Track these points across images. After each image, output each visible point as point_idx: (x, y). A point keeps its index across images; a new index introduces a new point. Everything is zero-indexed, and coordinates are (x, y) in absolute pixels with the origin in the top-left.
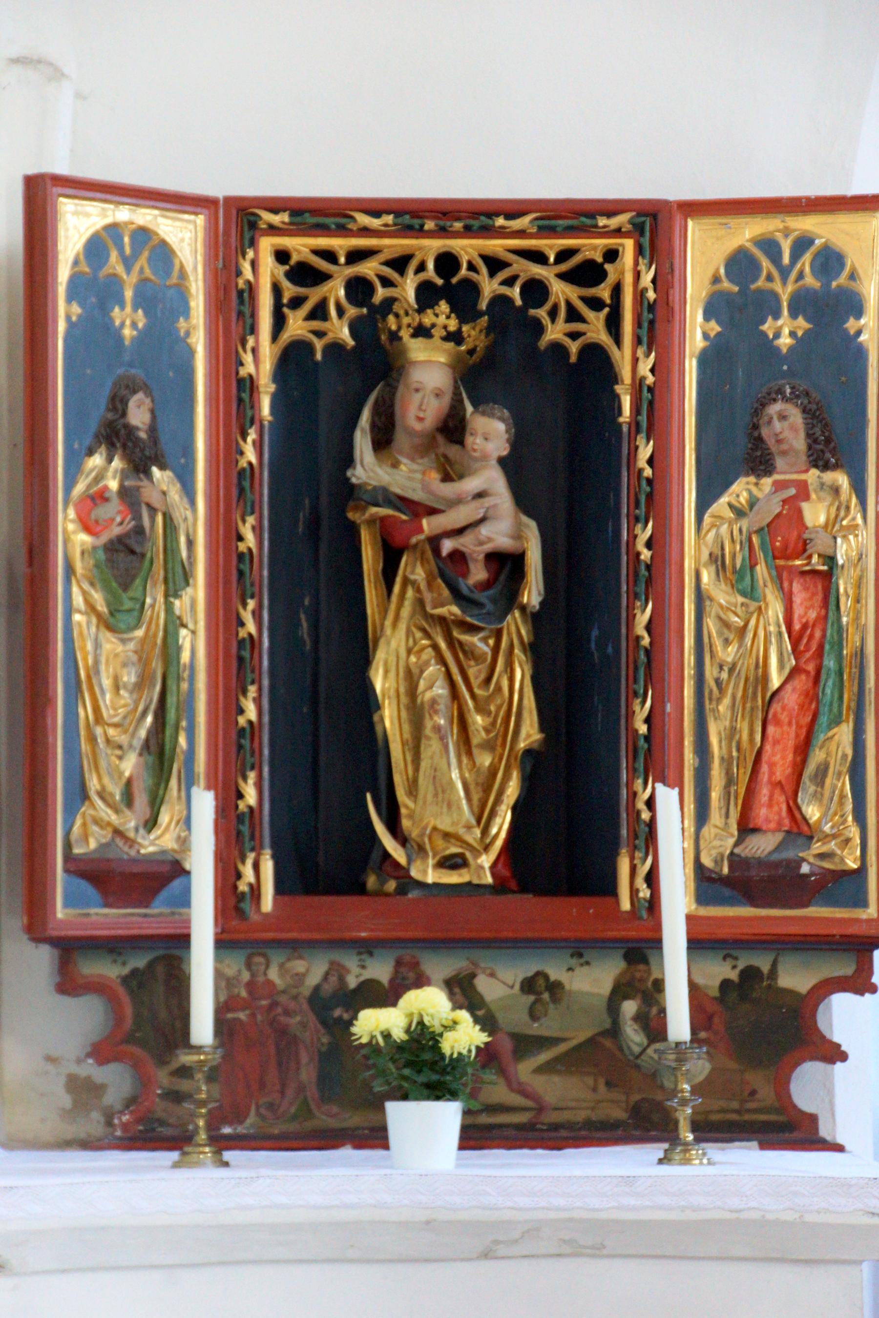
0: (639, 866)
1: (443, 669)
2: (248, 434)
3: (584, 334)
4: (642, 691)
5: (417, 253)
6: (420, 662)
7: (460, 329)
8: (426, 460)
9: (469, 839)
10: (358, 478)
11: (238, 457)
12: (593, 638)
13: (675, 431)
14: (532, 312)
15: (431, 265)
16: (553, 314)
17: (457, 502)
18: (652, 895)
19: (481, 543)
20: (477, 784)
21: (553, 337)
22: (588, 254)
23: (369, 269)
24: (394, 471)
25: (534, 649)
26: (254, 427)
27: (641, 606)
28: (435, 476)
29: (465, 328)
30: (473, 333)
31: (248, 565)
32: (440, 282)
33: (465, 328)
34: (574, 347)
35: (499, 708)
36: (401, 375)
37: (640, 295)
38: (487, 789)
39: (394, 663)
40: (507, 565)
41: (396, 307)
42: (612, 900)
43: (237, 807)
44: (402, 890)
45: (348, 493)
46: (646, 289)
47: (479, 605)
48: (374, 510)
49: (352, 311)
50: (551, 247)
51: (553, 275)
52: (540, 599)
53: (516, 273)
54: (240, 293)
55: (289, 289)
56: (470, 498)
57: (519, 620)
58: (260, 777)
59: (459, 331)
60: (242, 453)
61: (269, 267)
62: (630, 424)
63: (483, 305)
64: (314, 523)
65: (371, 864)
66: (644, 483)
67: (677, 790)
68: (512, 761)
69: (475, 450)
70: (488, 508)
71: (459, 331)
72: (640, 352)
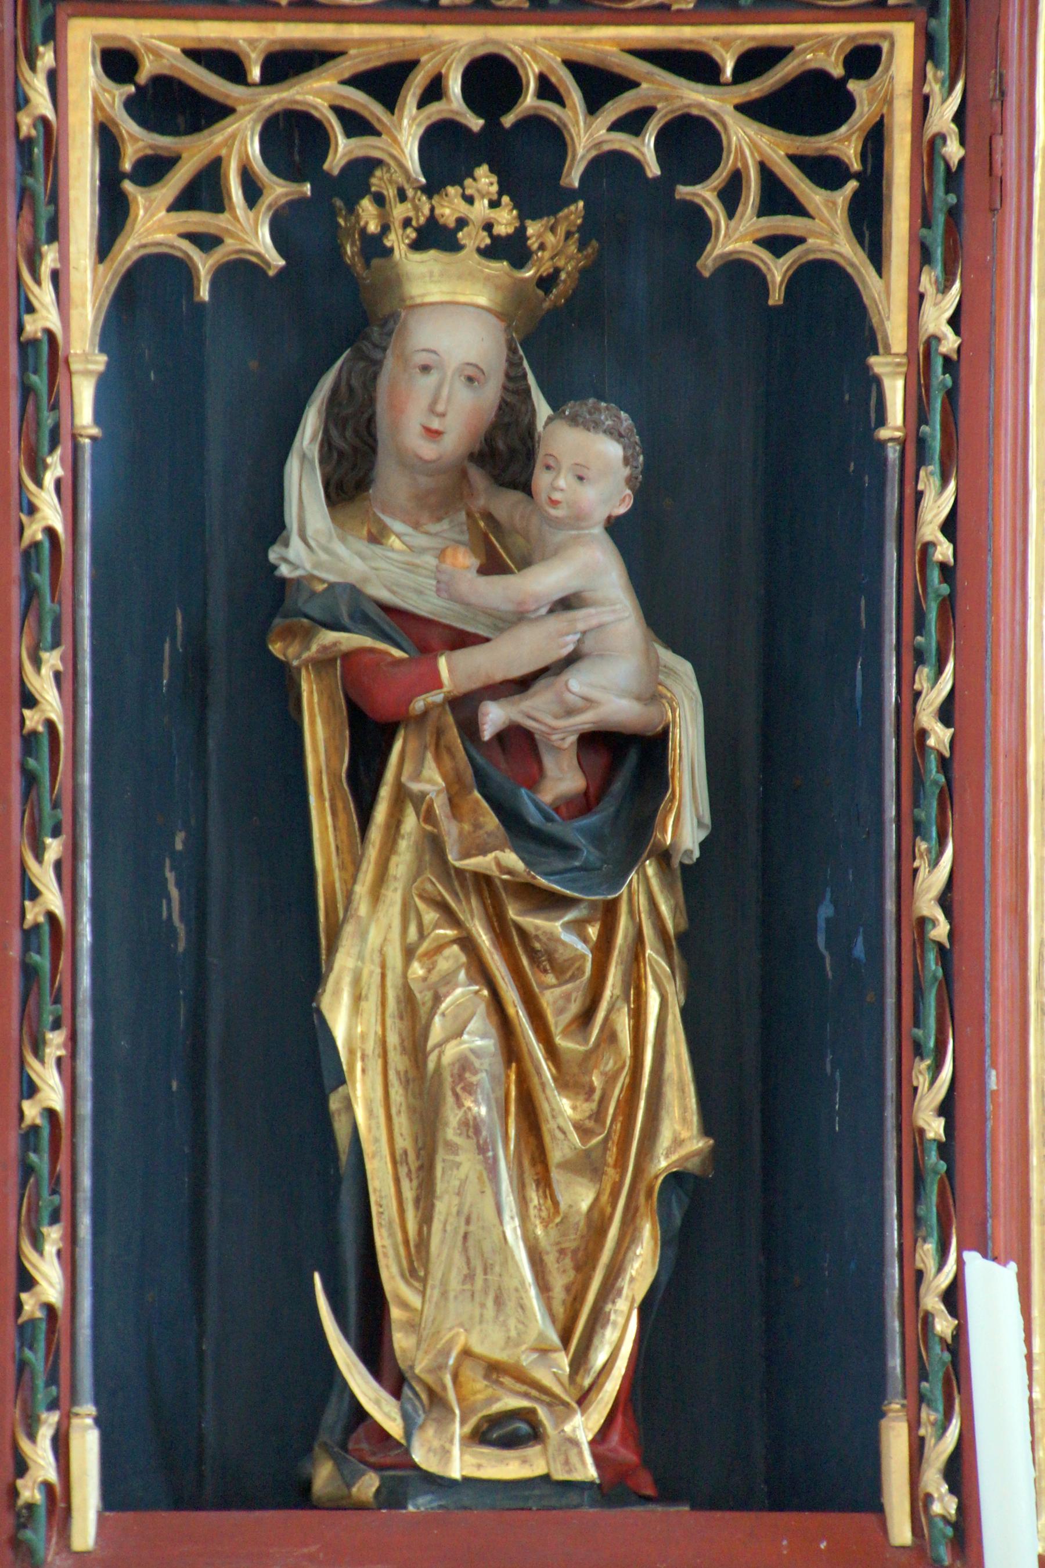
0: (930, 1442)
1: (485, 992)
2: (46, 467)
3: (801, 240)
4: (932, 1044)
5: (424, 58)
6: (434, 977)
7: (521, 231)
8: (445, 525)
9: (544, 1376)
10: (295, 566)
11: (24, 518)
12: (821, 924)
13: (1006, 457)
14: (684, 191)
15: (455, 86)
16: (731, 196)
17: (518, 618)
18: (960, 1509)
19: (570, 712)
20: (562, 1252)
21: (730, 248)
22: (812, 59)
23: (316, 93)
24: (377, 549)
25: (689, 948)
26: (58, 452)
27: (929, 851)
28: (465, 561)
29: (533, 229)
30: (550, 239)
31: (46, 1157)
32: (476, 123)
33: (533, 229)
34: (777, 271)
35: (611, 1079)
36: (390, 334)
37: (927, 150)
38: (584, 1265)
39: (376, 978)
40: (628, 758)
41: (377, 181)
42: (868, 1519)
43: (19, 1306)
44: (392, 1497)
45: (274, 599)
46: (943, 137)
47: (565, 848)
48: (329, 637)
49: (278, 190)
50: (726, 43)
51: (731, 108)
52: (702, 835)
53: (647, 103)
54: (25, 146)
55: (134, 139)
56: (543, 611)
57: (655, 883)
58: (72, 1238)
59: (520, 233)
60: (32, 510)
61: (89, 90)
62: (903, 443)
63: (573, 177)
64: (196, 663)
65: (324, 1437)
66: (935, 575)
67: (1013, 1267)
68: (642, 1199)
69: (554, 503)
70: (584, 633)
71: (520, 233)
72: (927, 282)
